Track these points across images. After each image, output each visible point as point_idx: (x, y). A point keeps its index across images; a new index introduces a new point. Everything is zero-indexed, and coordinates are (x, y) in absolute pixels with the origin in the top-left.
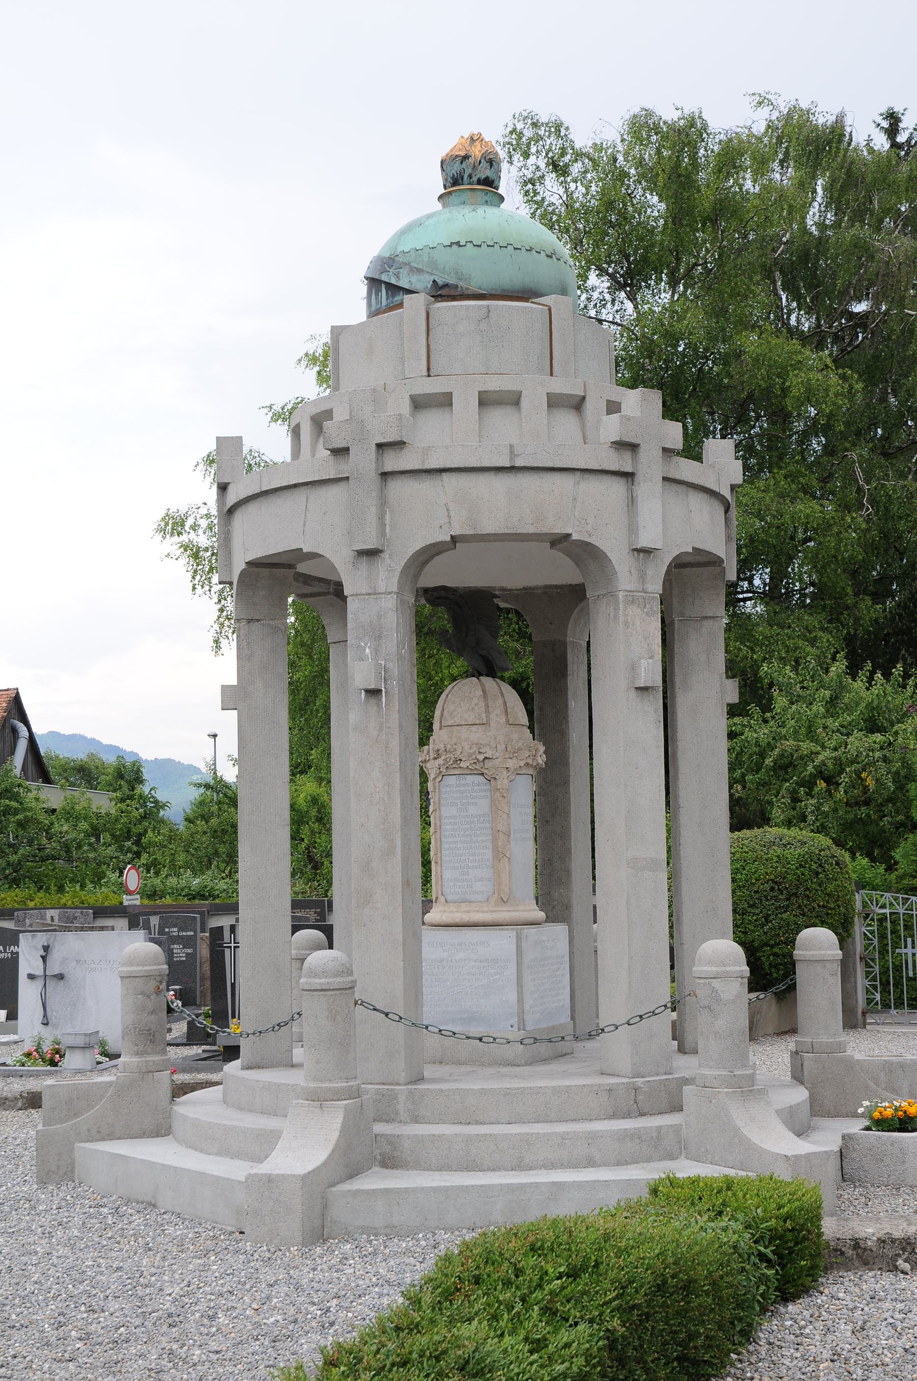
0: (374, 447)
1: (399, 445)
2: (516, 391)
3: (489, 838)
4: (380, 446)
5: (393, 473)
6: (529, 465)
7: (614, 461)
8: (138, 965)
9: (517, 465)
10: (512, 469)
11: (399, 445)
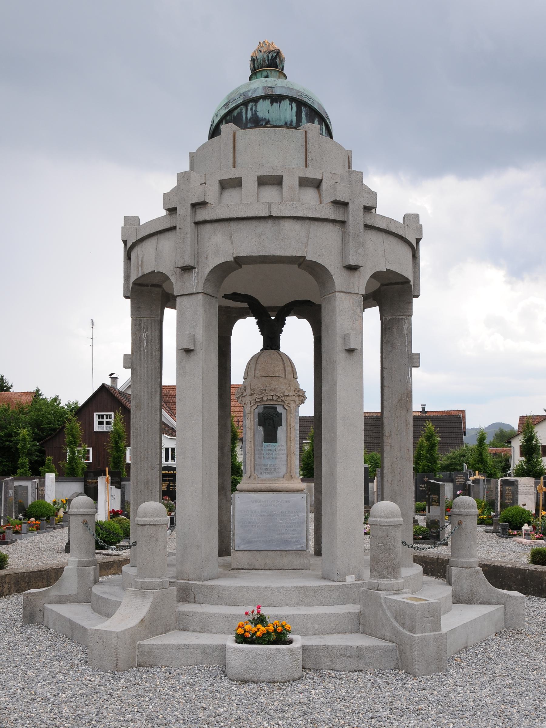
0: (189, 205)
1: (203, 204)
2: (238, 178)
3: (232, 408)
4: (194, 205)
5: (205, 222)
6: (240, 216)
7: (329, 212)
8: (85, 508)
9: (274, 214)
10: (270, 217)
11: (203, 204)
